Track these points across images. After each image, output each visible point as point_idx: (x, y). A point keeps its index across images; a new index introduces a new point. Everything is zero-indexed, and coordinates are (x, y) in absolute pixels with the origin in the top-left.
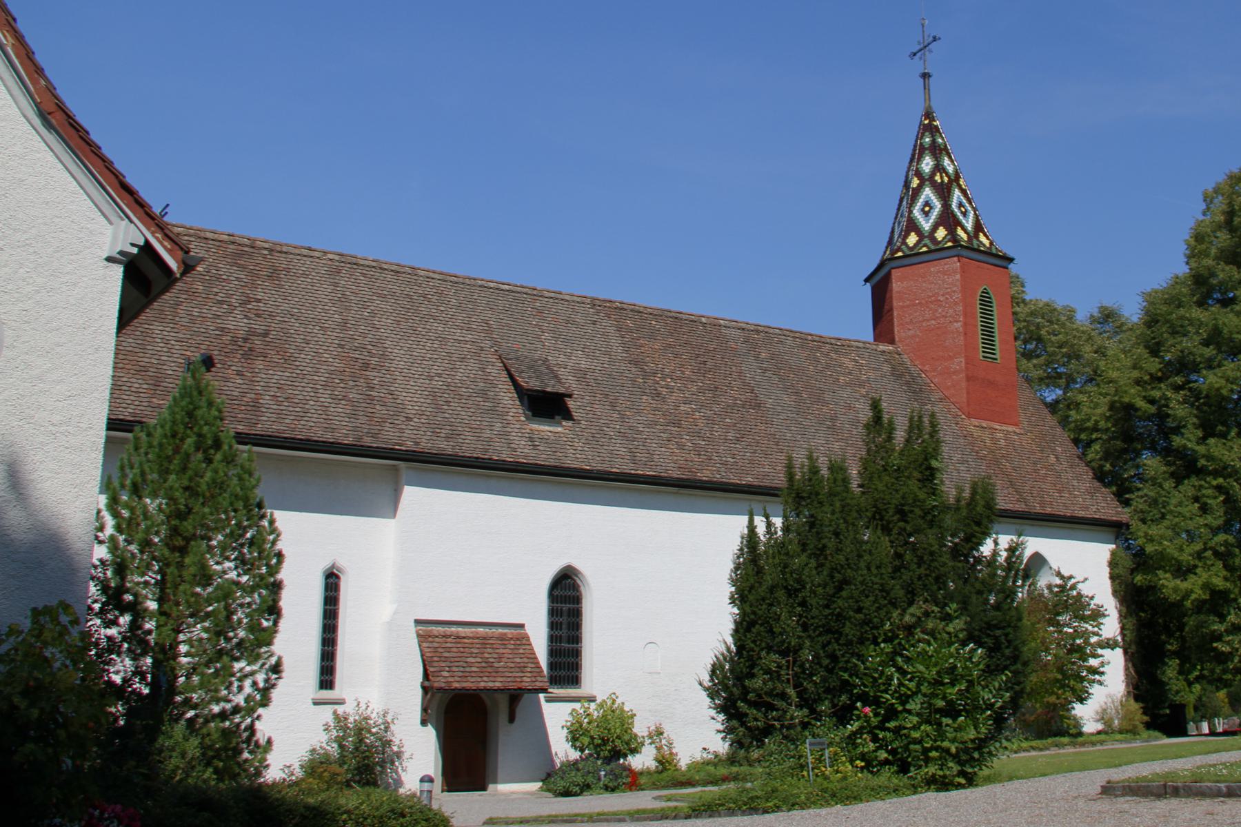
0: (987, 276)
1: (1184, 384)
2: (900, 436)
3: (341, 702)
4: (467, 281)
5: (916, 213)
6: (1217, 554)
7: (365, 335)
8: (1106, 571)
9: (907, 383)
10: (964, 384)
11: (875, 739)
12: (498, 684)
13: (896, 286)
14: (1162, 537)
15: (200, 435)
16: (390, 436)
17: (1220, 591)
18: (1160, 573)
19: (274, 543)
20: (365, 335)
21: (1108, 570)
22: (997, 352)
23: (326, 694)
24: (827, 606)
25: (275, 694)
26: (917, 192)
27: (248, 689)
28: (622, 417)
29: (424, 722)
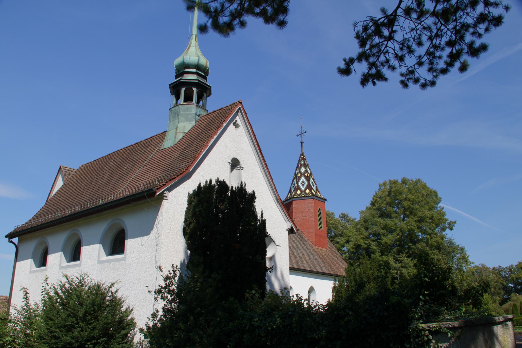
10: (314, 236)
26: (300, 177)
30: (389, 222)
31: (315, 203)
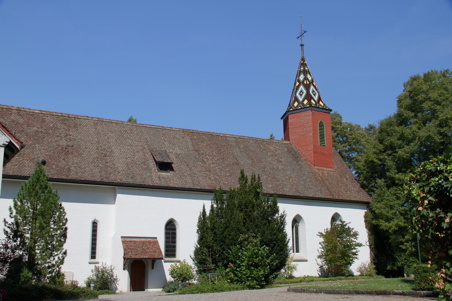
0: (322, 117)
1: (391, 153)
2: (249, 180)
3: (98, 263)
4: (140, 125)
5: (298, 95)
6: (401, 214)
7: (105, 145)
8: (363, 219)
9: (293, 155)
10: (313, 154)
11: (234, 274)
12: (147, 257)
13: (290, 120)
14: (381, 208)
15: (41, 185)
16: (113, 178)
17: (402, 227)
18: (380, 220)
19: (64, 216)
20: (105, 145)
21: (364, 219)
22: (325, 143)
23: (93, 260)
24: (222, 234)
25: (66, 260)
26: (298, 87)
27: (56, 258)
28: (191, 170)
29: (124, 269)
30: (407, 131)
31: (313, 115)
